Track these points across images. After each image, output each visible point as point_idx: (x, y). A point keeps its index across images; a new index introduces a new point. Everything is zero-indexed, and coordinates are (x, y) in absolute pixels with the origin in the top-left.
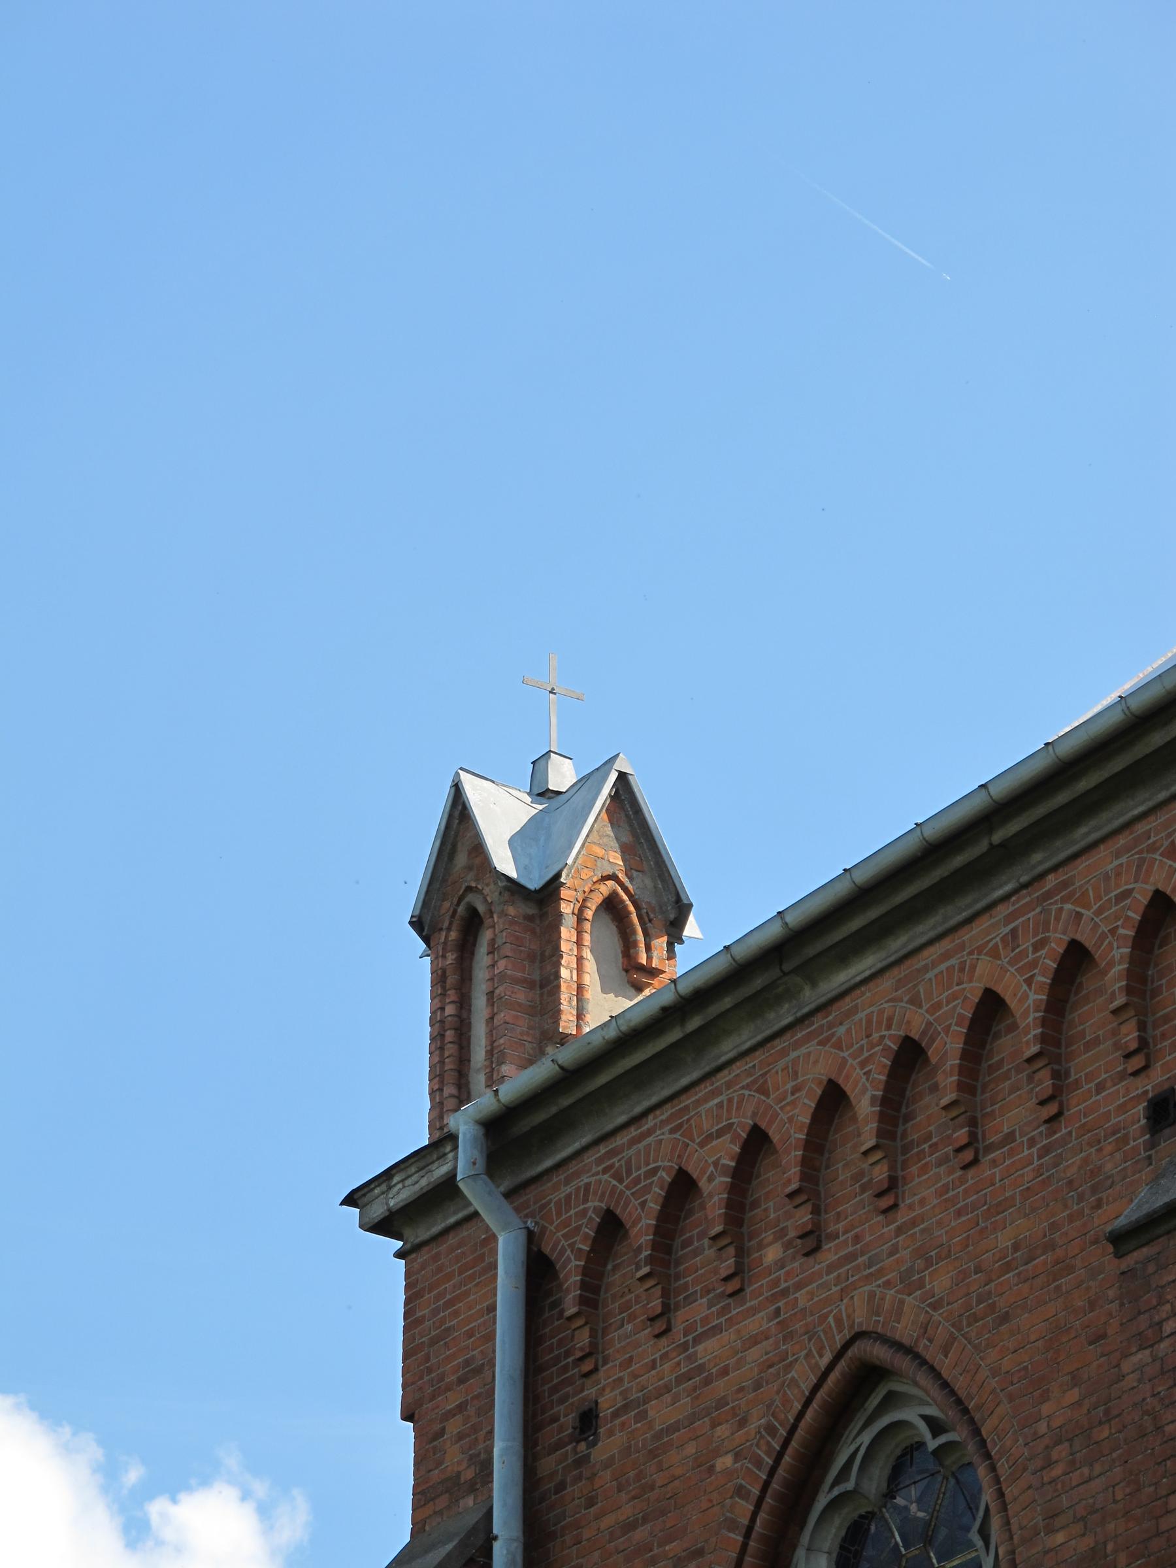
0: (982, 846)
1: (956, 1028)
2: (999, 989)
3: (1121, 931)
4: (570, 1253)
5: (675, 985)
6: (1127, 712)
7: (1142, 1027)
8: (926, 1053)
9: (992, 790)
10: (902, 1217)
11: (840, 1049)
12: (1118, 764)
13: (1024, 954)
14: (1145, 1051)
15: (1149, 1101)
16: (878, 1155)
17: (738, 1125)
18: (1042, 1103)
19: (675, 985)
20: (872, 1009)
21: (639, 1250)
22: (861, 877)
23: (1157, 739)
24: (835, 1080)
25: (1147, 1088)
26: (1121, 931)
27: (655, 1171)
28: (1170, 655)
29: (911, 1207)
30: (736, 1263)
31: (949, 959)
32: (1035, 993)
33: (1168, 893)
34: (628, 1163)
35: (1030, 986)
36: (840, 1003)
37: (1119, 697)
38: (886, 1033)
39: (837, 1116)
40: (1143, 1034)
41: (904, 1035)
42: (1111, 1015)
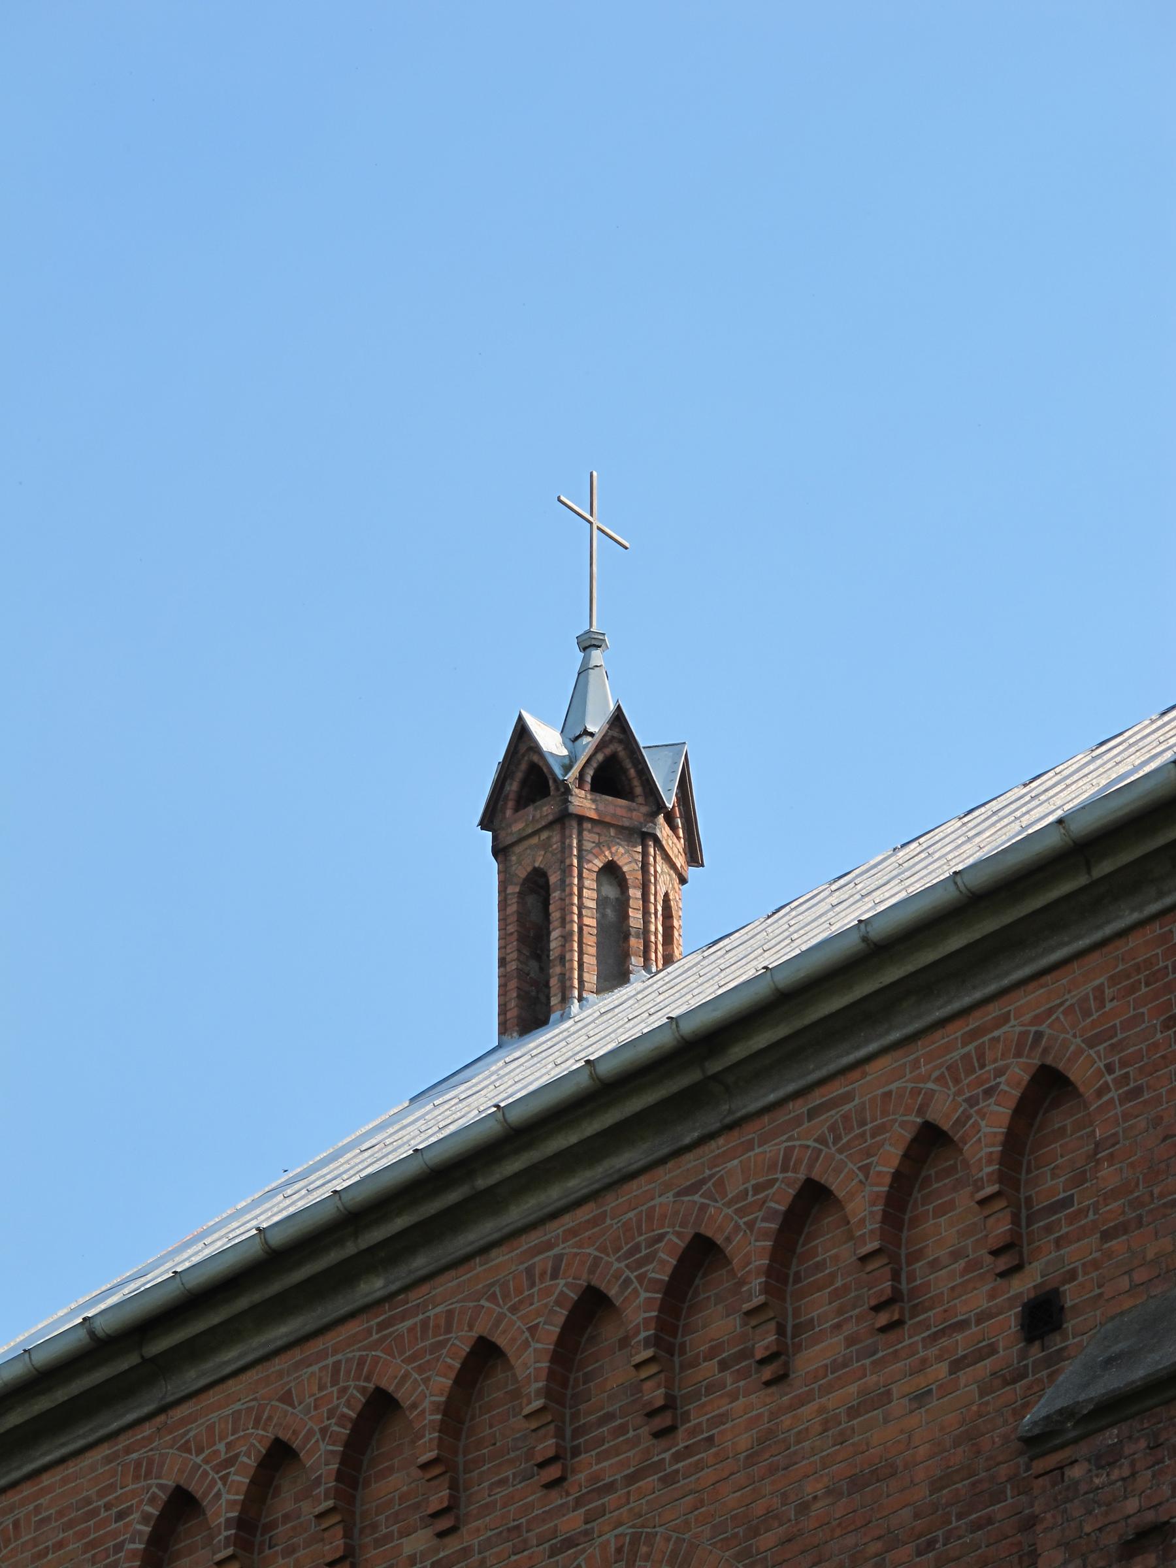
0: (132, 1360)
1: (420, 1389)
2: (192, 1488)
3: (760, 1224)
4: (222, 1487)
5: (30, 1355)
6: (342, 1209)
7: (347, 1534)
8: (299, 1456)
9: (344, 1196)
10: (682, 1440)
11: (189, 1451)
12: (61, 1395)
13: (637, 1248)
14: (350, 1559)
15: (1024, 1305)
16: (653, 1369)
17: (782, 1182)
18: (877, 1309)
19: (30, 1355)
20: (339, 1357)
21: (318, 1482)
22: (40, 1359)
23: (14, 1419)
24: (185, 1487)
25: (521, 1521)
26: (760, 1224)
27: (660, 1238)
28: (12, 1344)
29: (693, 1432)
30: (451, 1497)
31: (1000, 1027)
32: (646, 1291)
33: (602, 1289)
34: (211, 1429)
35: (224, 1485)
36: (634, 1184)
37: (765, 968)
38: (780, 1176)
39: (700, 1275)
40: (896, 1284)
41: (1040, 1063)
42: (977, 1206)
